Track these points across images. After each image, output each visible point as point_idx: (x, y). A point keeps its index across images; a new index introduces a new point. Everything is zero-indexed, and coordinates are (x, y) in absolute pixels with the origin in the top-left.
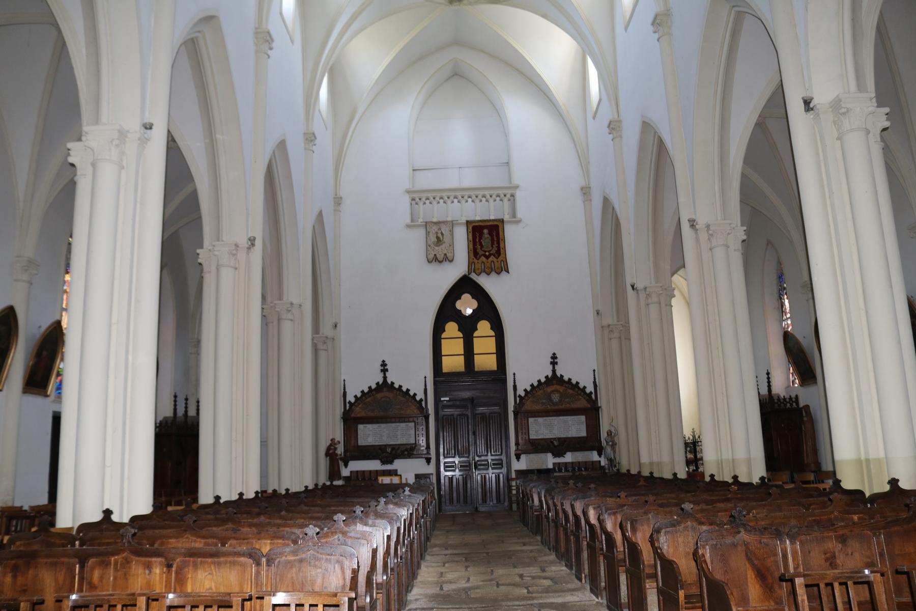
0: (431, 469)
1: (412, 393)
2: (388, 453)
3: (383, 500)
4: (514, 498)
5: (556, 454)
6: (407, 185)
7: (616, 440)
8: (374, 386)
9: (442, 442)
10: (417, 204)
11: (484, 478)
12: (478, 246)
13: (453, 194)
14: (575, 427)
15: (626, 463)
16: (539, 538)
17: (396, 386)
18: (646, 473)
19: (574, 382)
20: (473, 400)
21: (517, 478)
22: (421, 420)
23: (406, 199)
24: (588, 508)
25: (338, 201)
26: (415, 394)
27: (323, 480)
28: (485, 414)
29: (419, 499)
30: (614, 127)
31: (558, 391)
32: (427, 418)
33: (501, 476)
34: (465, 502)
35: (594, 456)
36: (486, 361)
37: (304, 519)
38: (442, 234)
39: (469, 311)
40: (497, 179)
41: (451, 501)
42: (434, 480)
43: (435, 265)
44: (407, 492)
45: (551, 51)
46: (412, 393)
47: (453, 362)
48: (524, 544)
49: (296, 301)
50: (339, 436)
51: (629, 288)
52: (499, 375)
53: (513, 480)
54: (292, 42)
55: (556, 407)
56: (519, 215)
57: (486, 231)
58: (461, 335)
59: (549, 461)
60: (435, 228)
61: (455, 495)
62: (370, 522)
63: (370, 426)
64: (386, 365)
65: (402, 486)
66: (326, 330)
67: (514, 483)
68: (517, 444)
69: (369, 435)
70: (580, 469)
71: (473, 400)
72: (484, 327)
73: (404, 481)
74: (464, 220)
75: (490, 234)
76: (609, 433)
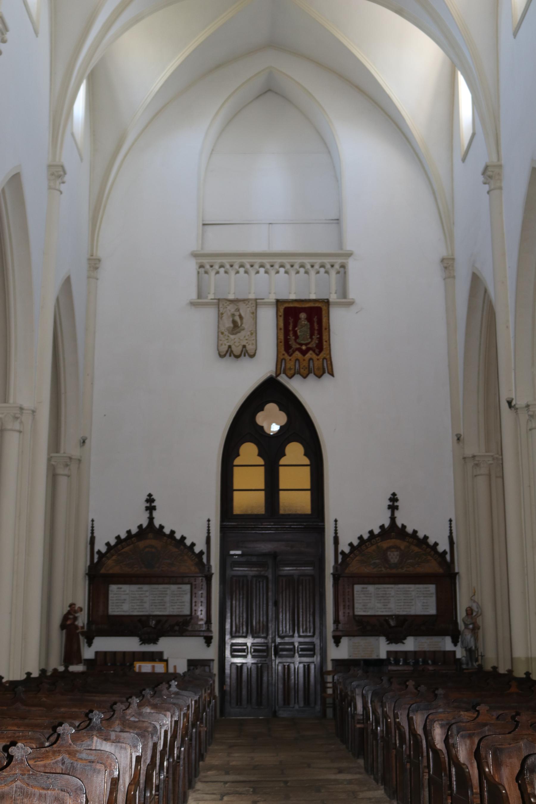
0: (211, 653)
1: (188, 542)
2: (151, 628)
3: (135, 701)
4: (329, 701)
5: (391, 640)
6: (194, 246)
7: (479, 621)
8: (134, 530)
9: (228, 615)
10: (206, 272)
11: (287, 670)
12: (291, 337)
13: (258, 261)
14: (420, 600)
15: (492, 657)
16: (361, 762)
17: (167, 531)
18: (520, 673)
19: (421, 535)
20: (275, 551)
21: (334, 672)
22: (200, 581)
23: (192, 266)
24: (432, 725)
25: (94, 264)
26: (193, 545)
27: (55, 663)
28: (292, 576)
29: (190, 700)
30: (491, 174)
31: (397, 548)
32: (209, 578)
33: (312, 667)
34: (259, 703)
35: (447, 644)
36: (295, 499)
37: (18, 726)
38: (241, 317)
39: (275, 428)
40: (321, 243)
41: (239, 701)
42: (215, 669)
43: (228, 361)
44: (174, 689)
45: (408, 63)
46: (188, 542)
47: (249, 499)
48: (340, 771)
49: (27, 404)
50: (81, 600)
51: (504, 405)
52: (315, 519)
53: (329, 673)
54: (36, 33)
55: (394, 571)
56: (352, 295)
57: (303, 316)
58: (262, 462)
59: (382, 648)
60: (231, 308)
61: (244, 692)
62: (113, 735)
63: (126, 588)
64: (153, 501)
65: (167, 678)
66: (70, 447)
67: (329, 679)
68: (336, 621)
69: (125, 600)
70: (425, 662)
71: (275, 551)
72: (295, 452)
73: (171, 670)
74: (272, 298)
75: (309, 319)
76: (470, 612)
